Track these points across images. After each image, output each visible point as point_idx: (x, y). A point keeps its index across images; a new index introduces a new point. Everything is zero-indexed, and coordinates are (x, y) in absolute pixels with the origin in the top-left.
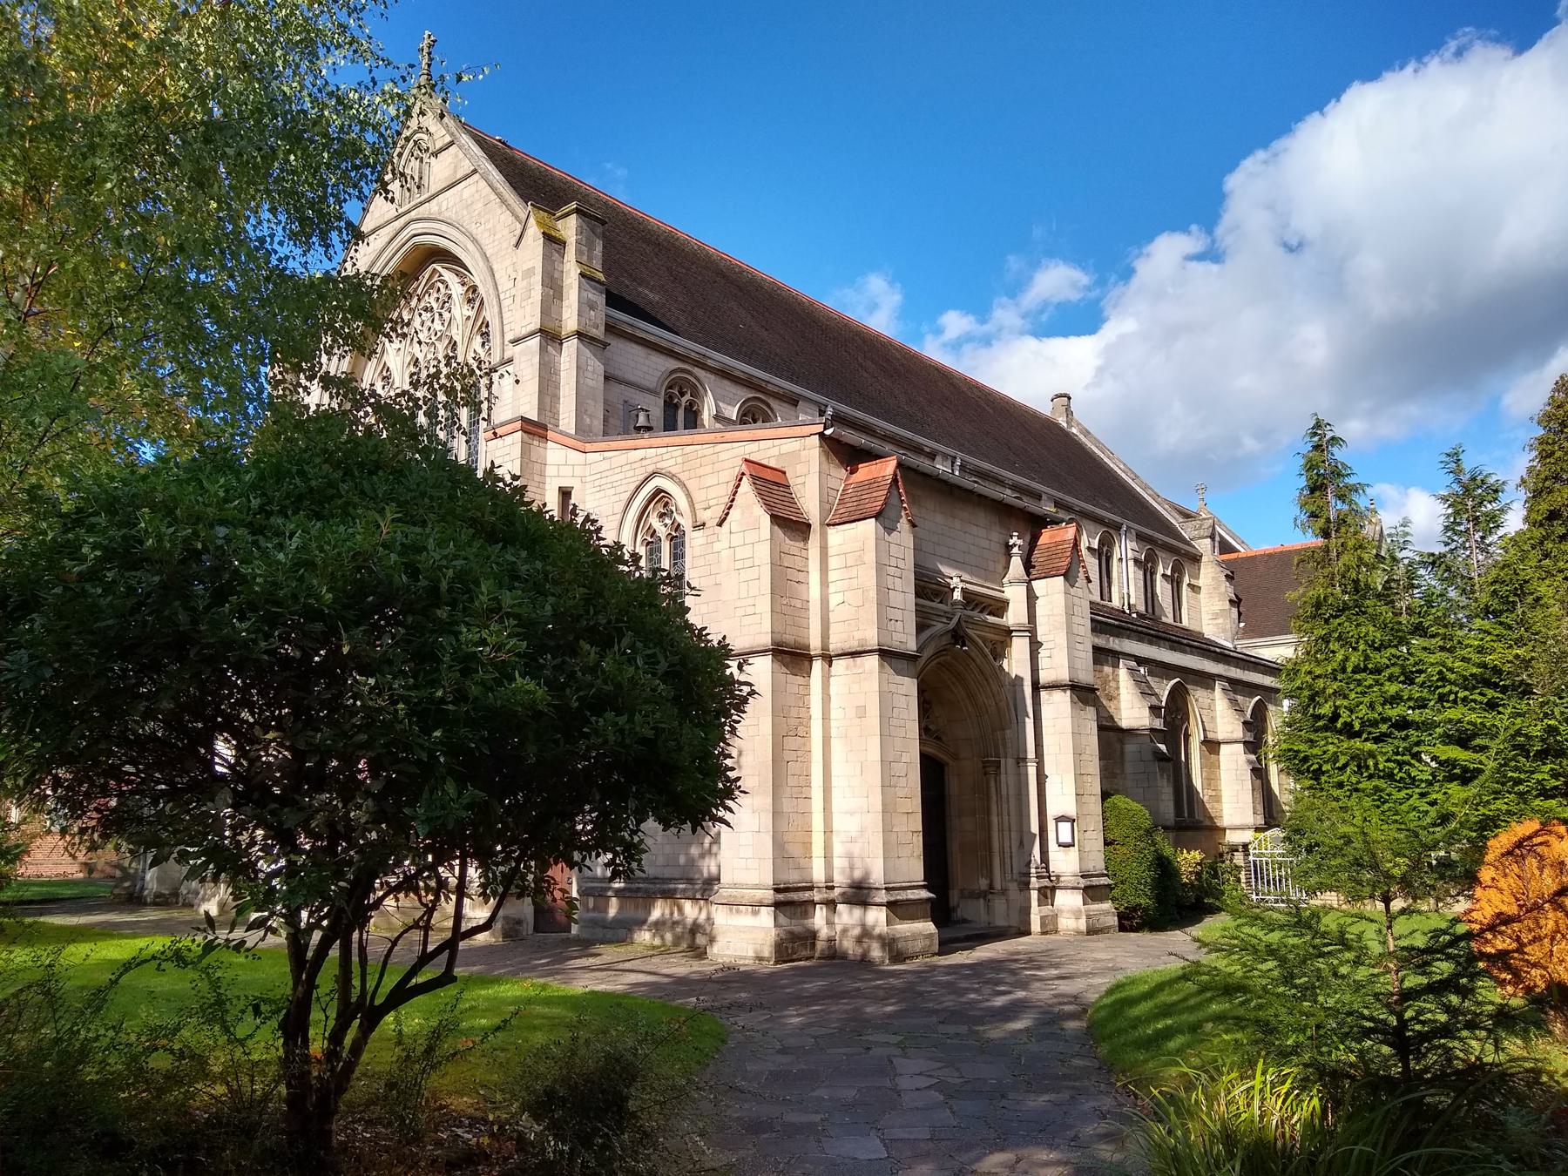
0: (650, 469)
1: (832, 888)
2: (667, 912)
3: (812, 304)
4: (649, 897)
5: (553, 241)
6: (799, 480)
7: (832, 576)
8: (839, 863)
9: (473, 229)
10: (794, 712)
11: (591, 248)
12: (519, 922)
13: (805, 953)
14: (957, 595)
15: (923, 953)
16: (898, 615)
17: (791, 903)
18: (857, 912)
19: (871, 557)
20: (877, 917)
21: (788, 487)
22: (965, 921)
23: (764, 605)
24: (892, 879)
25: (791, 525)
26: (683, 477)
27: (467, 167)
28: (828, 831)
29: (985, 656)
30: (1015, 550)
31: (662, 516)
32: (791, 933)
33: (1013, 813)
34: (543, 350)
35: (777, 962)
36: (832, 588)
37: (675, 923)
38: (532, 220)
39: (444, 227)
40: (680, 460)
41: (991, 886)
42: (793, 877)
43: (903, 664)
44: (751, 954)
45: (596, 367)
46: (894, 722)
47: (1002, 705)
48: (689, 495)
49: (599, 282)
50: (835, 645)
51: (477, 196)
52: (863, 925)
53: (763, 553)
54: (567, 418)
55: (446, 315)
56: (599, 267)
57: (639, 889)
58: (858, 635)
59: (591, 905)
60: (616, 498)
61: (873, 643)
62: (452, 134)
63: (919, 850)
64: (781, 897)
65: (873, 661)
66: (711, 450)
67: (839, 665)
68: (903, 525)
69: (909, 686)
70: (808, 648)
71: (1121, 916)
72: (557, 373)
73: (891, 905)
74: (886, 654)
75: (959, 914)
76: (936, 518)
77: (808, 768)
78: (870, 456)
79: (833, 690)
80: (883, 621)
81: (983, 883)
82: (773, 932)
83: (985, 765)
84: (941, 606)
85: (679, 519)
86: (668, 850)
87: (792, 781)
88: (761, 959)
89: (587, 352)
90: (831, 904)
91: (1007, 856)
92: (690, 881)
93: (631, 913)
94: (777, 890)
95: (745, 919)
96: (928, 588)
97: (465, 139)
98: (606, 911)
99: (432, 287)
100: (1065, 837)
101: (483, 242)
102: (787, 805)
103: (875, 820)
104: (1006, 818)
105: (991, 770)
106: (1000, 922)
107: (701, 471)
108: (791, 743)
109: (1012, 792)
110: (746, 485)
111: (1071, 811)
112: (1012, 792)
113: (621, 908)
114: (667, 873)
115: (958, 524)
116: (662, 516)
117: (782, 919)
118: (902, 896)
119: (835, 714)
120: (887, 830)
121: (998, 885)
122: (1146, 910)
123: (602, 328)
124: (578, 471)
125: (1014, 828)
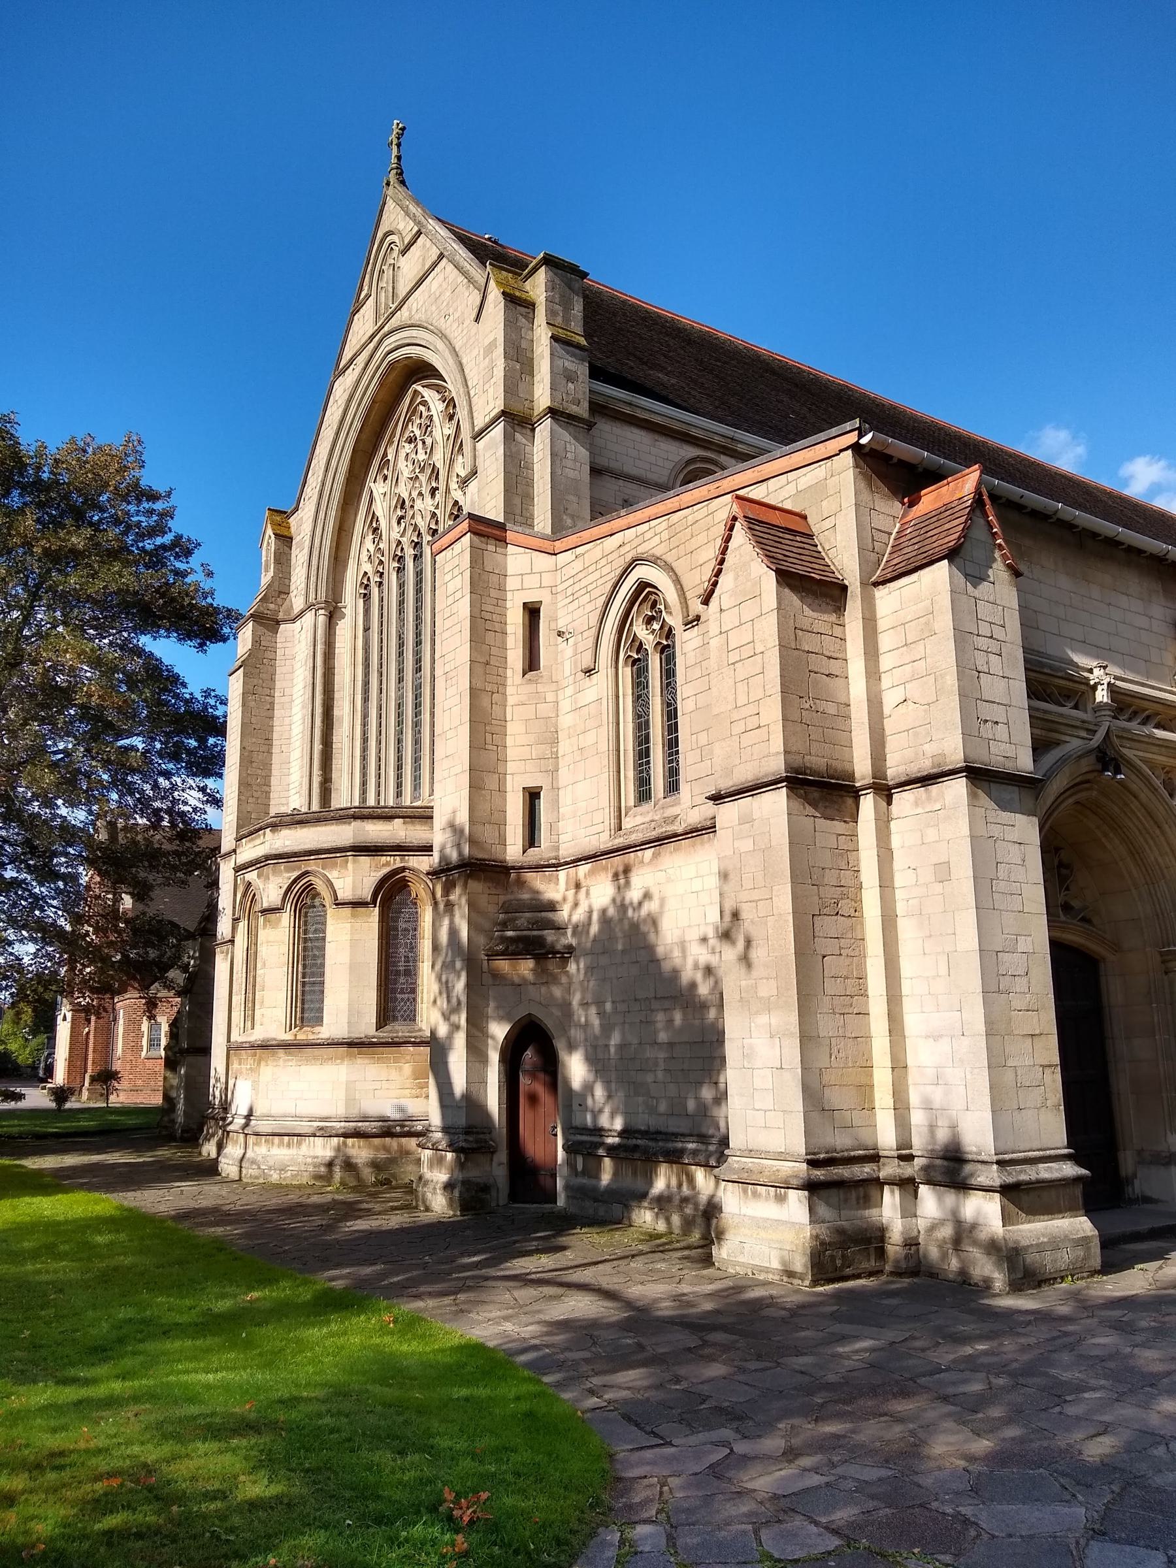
0: (629, 558)
1: (909, 1158)
2: (674, 1182)
4: (648, 1160)
5: (517, 304)
6: (828, 524)
7: (885, 662)
8: (918, 1118)
9: (442, 324)
10: (830, 878)
11: (567, 306)
12: (485, 1188)
13: (866, 1265)
14: (1102, 695)
15: (1074, 1272)
16: (998, 713)
18: (950, 1197)
19: (944, 622)
20: (985, 1210)
21: (811, 536)
22: (1147, 1200)
23: (773, 712)
24: (1010, 1145)
25: (810, 584)
26: (669, 558)
27: (434, 253)
28: (899, 1067)
29: (1154, 790)
31: (649, 620)
32: (840, 1231)
34: (508, 438)
35: (815, 1282)
36: (886, 682)
37: (685, 1200)
38: (492, 283)
39: (414, 333)
40: (665, 535)
42: (841, 1142)
43: (1012, 793)
44: (776, 1265)
45: (579, 454)
46: (1001, 886)
48: (677, 581)
49: (578, 346)
50: (895, 769)
51: (445, 285)
52: (958, 1223)
53: (768, 631)
54: (543, 519)
55: (429, 441)
56: (580, 330)
57: (636, 1147)
58: (930, 749)
59: (580, 1167)
60: (589, 607)
61: (956, 758)
62: (418, 223)
63: (1055, 1094)
64: (819, 1174)
65: (958, 787)
66: (704, 512)
67: (903, 801)
68: (998, 571)
69: (1023, 832)
70: (851, 776)
72: (529, 467)
73: (1007, 1190)
74: (979, 775)
75: (1139, 1187)
76: (1059, 581)
77: (862, 966)
78: (935, 476)
79: (896, 842)
80: (973, 721)
82: (807, 1232)
84: (1074, 713)
85: (670, 621)
86: (672, 1090)
87: (831, 987)
88: (791, 1274)
89: (565, 435)
90: (907, 1185)
92: (703, 1138)
93: (630, 1182)
94: (813, 1163)
95: (763, 1208)
96: (1050, 685)
97: (432, 225)
98: (597, 1177)
99: (413, 413)
101: (451, 336)
102: (826, 1026)
103: (975, 1047)
107: (694, 544)
108: (828, 925)
110: (740, 535)
113: (616, 1174)
114: (673, 1126)
115: (1095, 592)
116: (649, 620)
117: (823, 1210)
118: (1028, 1174)
119: (901, 878)
120: (996, 1064)
123: (586, 405)
124: (547, 580)
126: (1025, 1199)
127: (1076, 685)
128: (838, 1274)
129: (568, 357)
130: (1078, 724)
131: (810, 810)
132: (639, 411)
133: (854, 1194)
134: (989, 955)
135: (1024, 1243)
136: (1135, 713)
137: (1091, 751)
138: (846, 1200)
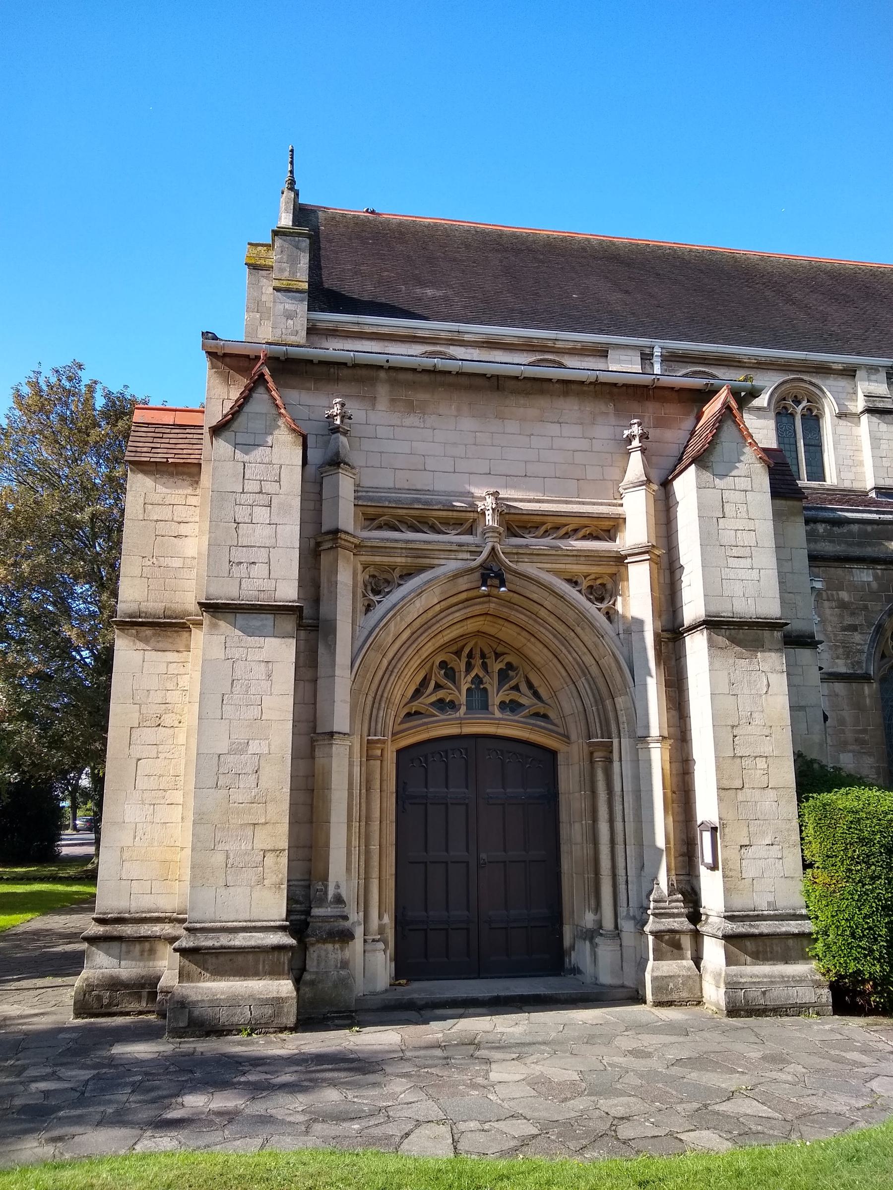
3: (712, 252)
14: (490, 520)
17: (119, 939)
22: (576, 971)
30: (636, 443)
33: (629, 817)
49: (298, 291)
56: (305, 278)
71: (833, 987)
75: (574, 958)
81: (589, 919)
91: (621, 879)
100: (708, 859)
104: (619, 825)
105: (598, 756)
106: (606, 978)
111: (716, 821)
115: (512, 426)
121: (608, 924)
122: (881, 983)
123: (304, 333)
125: (631, 840)
126: (212, 960)
127: (463, 514)
128: (103, 1010)
129: (288, 301)
130: (455, 548)
131: (140, 645)
132: (366, 327)
133: (138, 947)
135: (194, 998)
136: (557, 528)
137: (472, 570)
138: (128, 952)
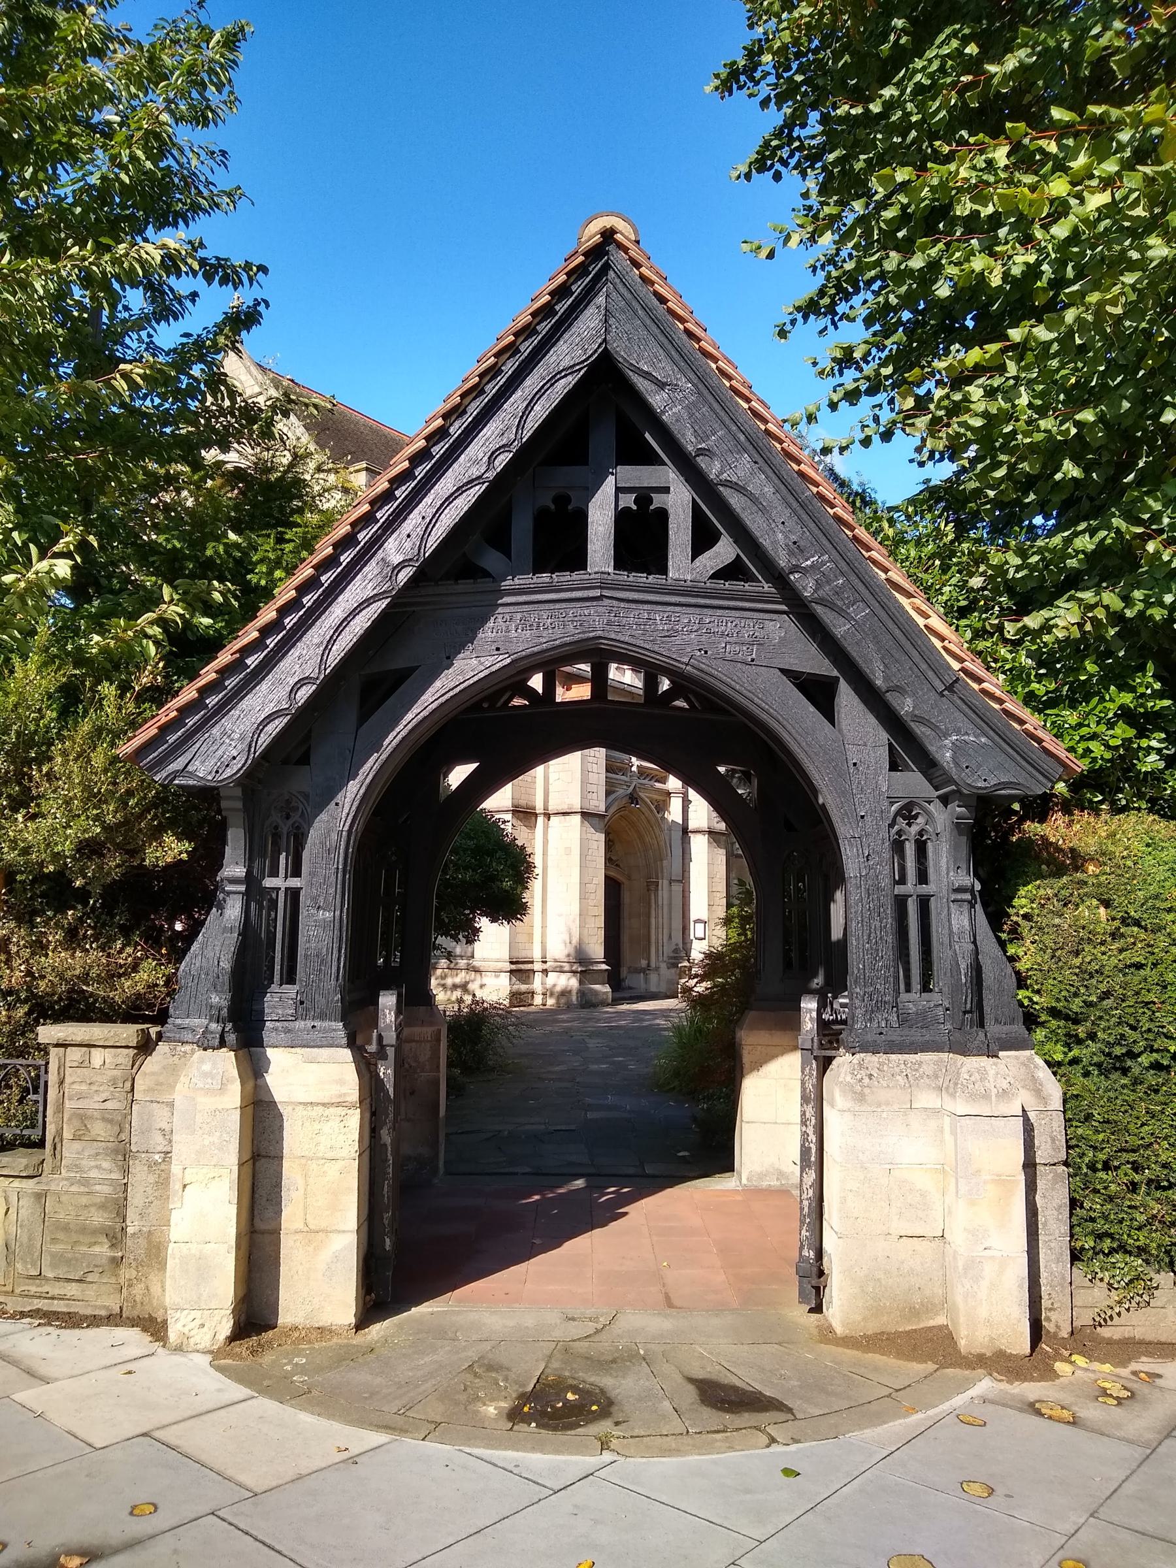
14: (634, 769)
22: (630, 988)
41: (649, 965)
47: (662, 843)
64: (513, 967)
65: (578, 818)
69: (598, 840)
74: (585, 815)
75: (627, 983)
80: (585, 793)
81: (644, 963)
83: (649, 884)
105: (653, 888)
109: (665, 902)
111: (705, 917)
112: (665, 902)
121: (653, 965)
134: (583, 884)
